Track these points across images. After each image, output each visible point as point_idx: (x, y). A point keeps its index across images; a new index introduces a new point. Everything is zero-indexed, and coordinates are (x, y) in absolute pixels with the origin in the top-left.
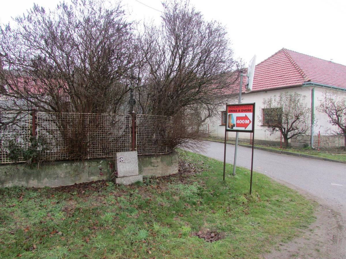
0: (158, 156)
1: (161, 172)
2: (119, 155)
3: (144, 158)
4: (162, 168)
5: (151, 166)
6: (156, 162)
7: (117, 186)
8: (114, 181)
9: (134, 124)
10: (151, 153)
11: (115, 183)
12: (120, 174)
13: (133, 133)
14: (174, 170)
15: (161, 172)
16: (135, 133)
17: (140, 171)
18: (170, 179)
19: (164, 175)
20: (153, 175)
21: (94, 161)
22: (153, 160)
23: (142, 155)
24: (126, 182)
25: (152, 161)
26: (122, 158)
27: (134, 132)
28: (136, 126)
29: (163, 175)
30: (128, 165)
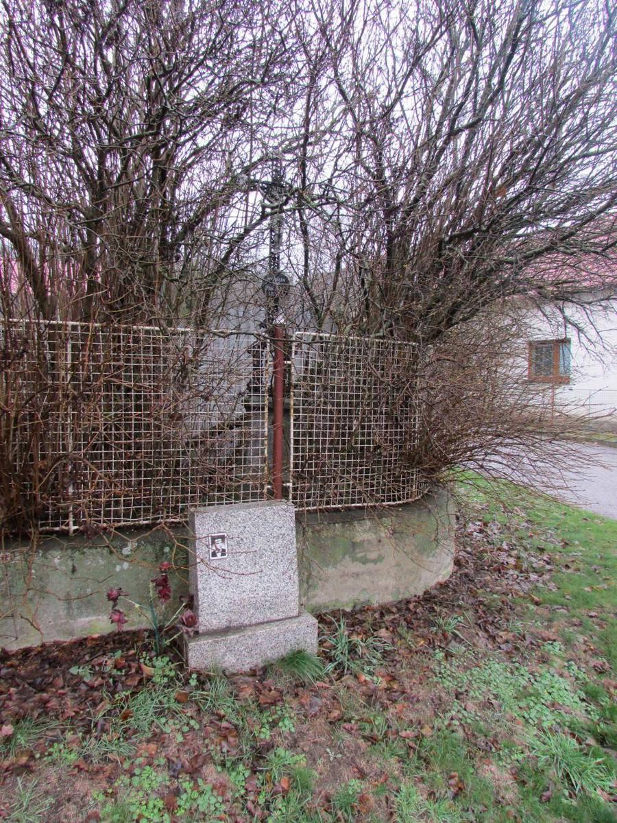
0: (377, 513)
1: (391, 582)
2: (209, 522)
3: (323, 519)
4: (398, 565)
5: (354, 560)
6: (375, 542)
7: (193, 683)
8: (177, 651)
9: (280, 377)
10: (353, 501)
11: (181, 668)
12: (208, 618)
13: (279, 412)
14: (439, 568)
15: (391, 582)
16: (286, 411)
17: (307, 580)
18: (440, 626)
19: (407, 596)
20: (363, 598)
21: (94, 546)
22: (363, 532)
23: (315, 511)
24: (233, 656)
25: (358, 539)
26: (223, 538)
27: (279, 409)
28: (290, 384)
29: (401, 597)
30: (252, 572)
